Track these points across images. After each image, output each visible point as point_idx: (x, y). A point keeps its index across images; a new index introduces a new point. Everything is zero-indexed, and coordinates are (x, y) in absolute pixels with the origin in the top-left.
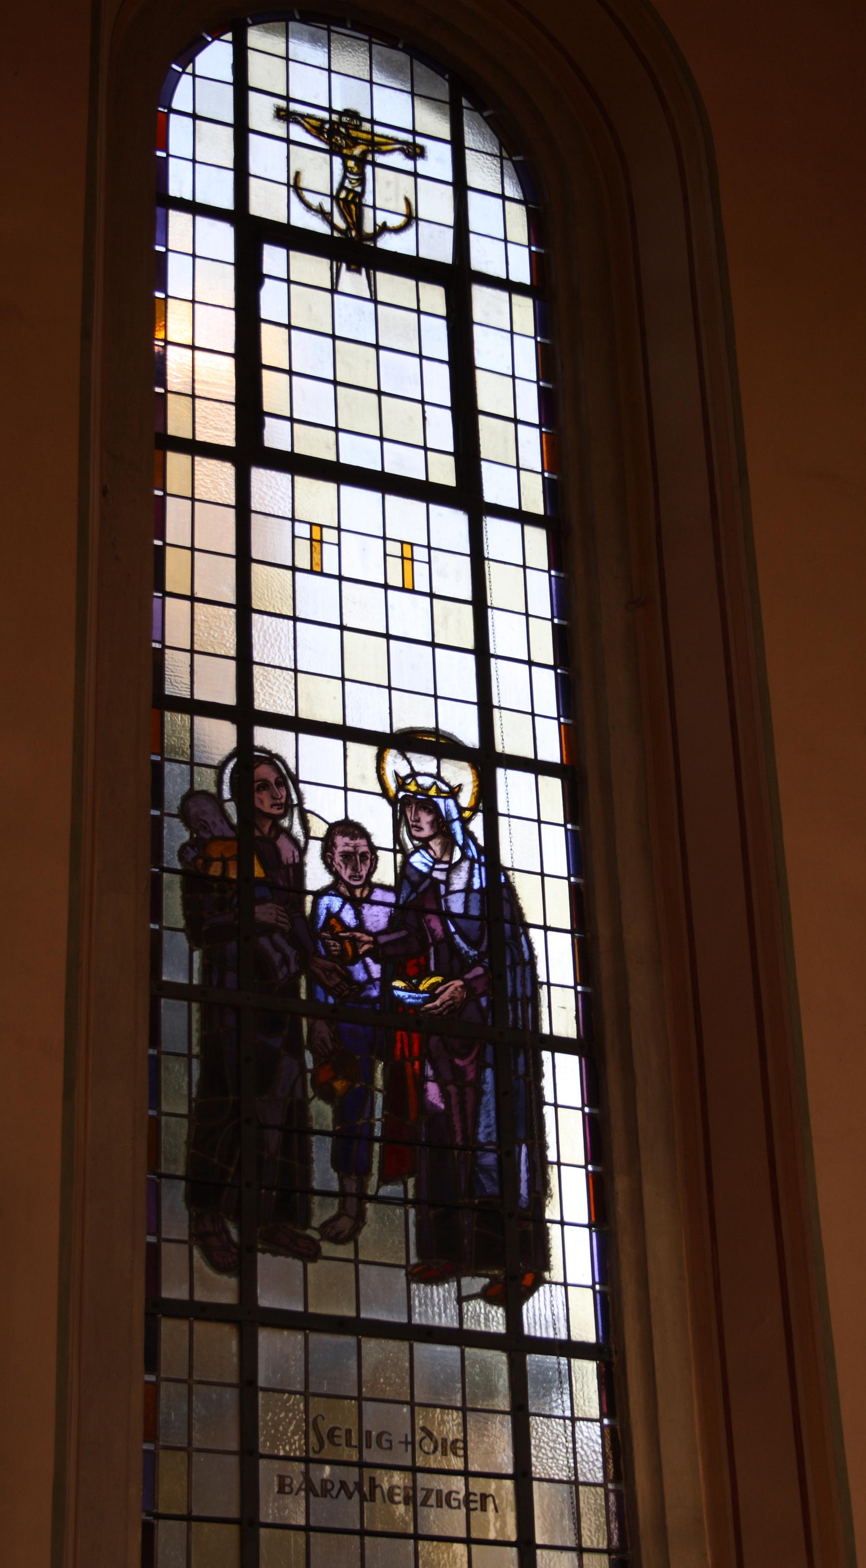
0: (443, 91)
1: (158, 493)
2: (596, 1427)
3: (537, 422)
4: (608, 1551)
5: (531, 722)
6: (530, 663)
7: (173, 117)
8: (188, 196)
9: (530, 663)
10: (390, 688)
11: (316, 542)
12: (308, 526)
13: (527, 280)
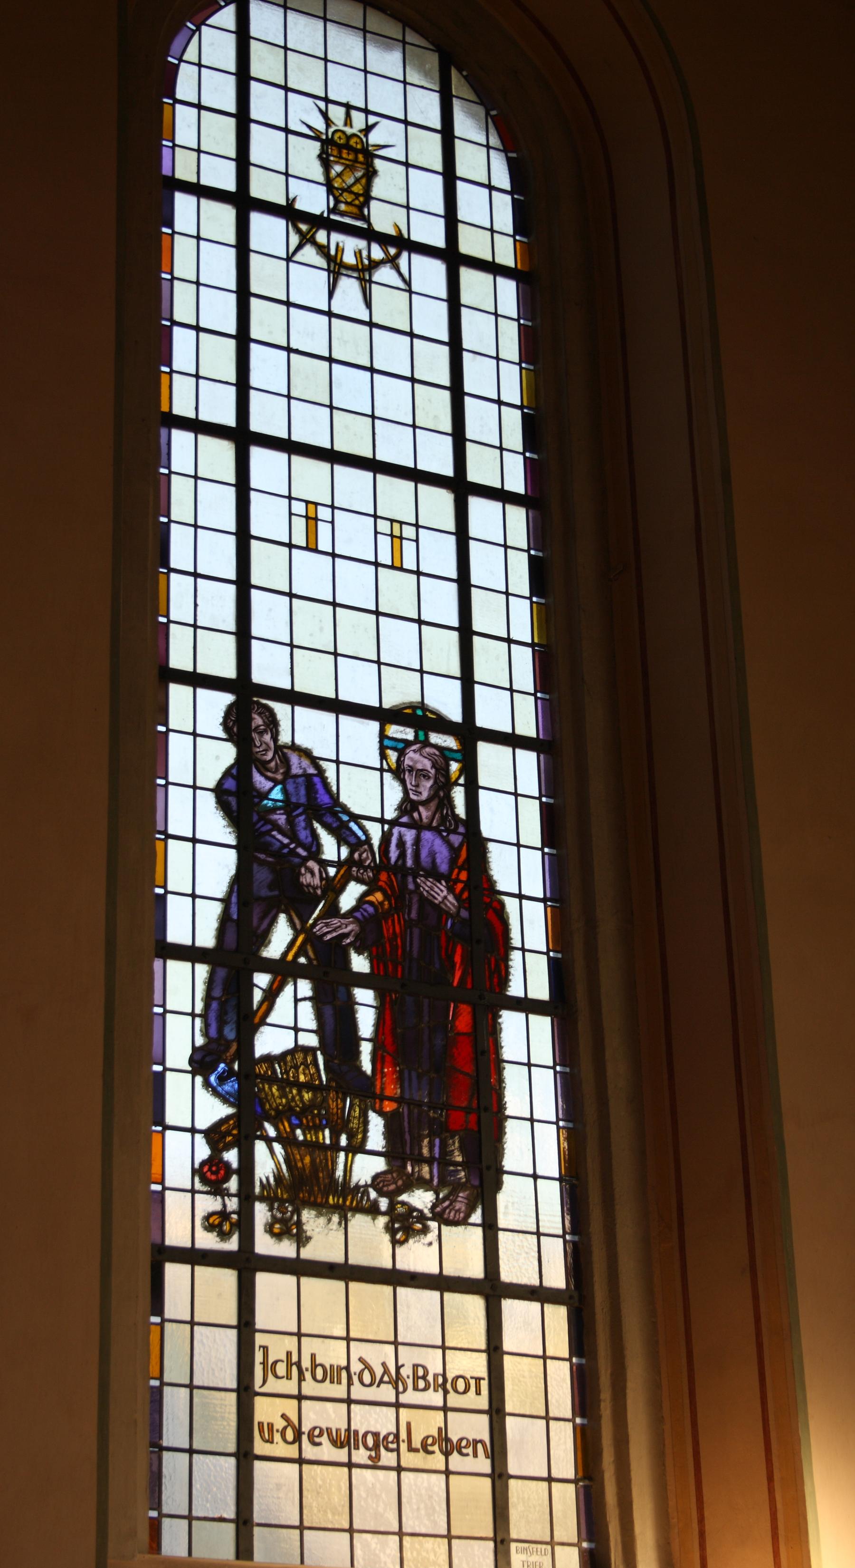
0: (433, 60)
1: (164, 520)
2: (575, 1551)
3: (508, 188)
4: (532, 645)
5: (509, 702)
6: (509, 641)
7: (176, 330)
8: (191, 415)
9: (499, 402)
10: (379, 663)
11: (312, 520)
12: (304, 504)
13: (521, 490)
